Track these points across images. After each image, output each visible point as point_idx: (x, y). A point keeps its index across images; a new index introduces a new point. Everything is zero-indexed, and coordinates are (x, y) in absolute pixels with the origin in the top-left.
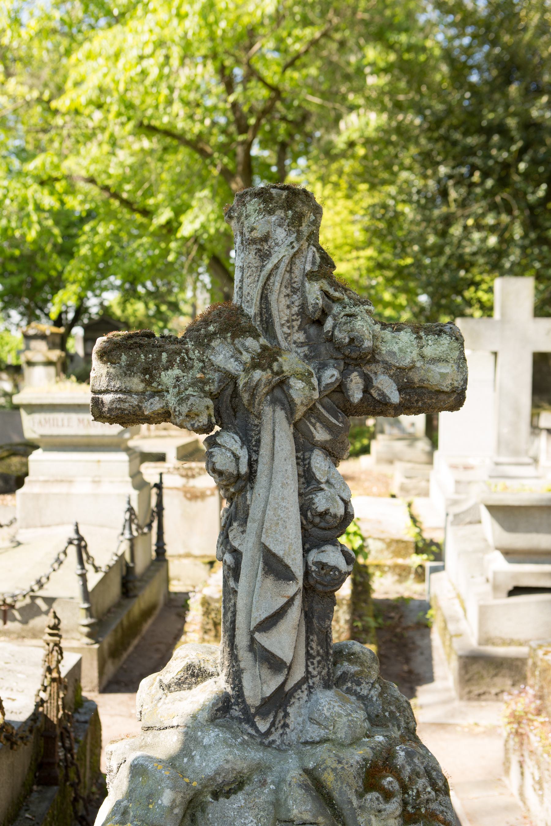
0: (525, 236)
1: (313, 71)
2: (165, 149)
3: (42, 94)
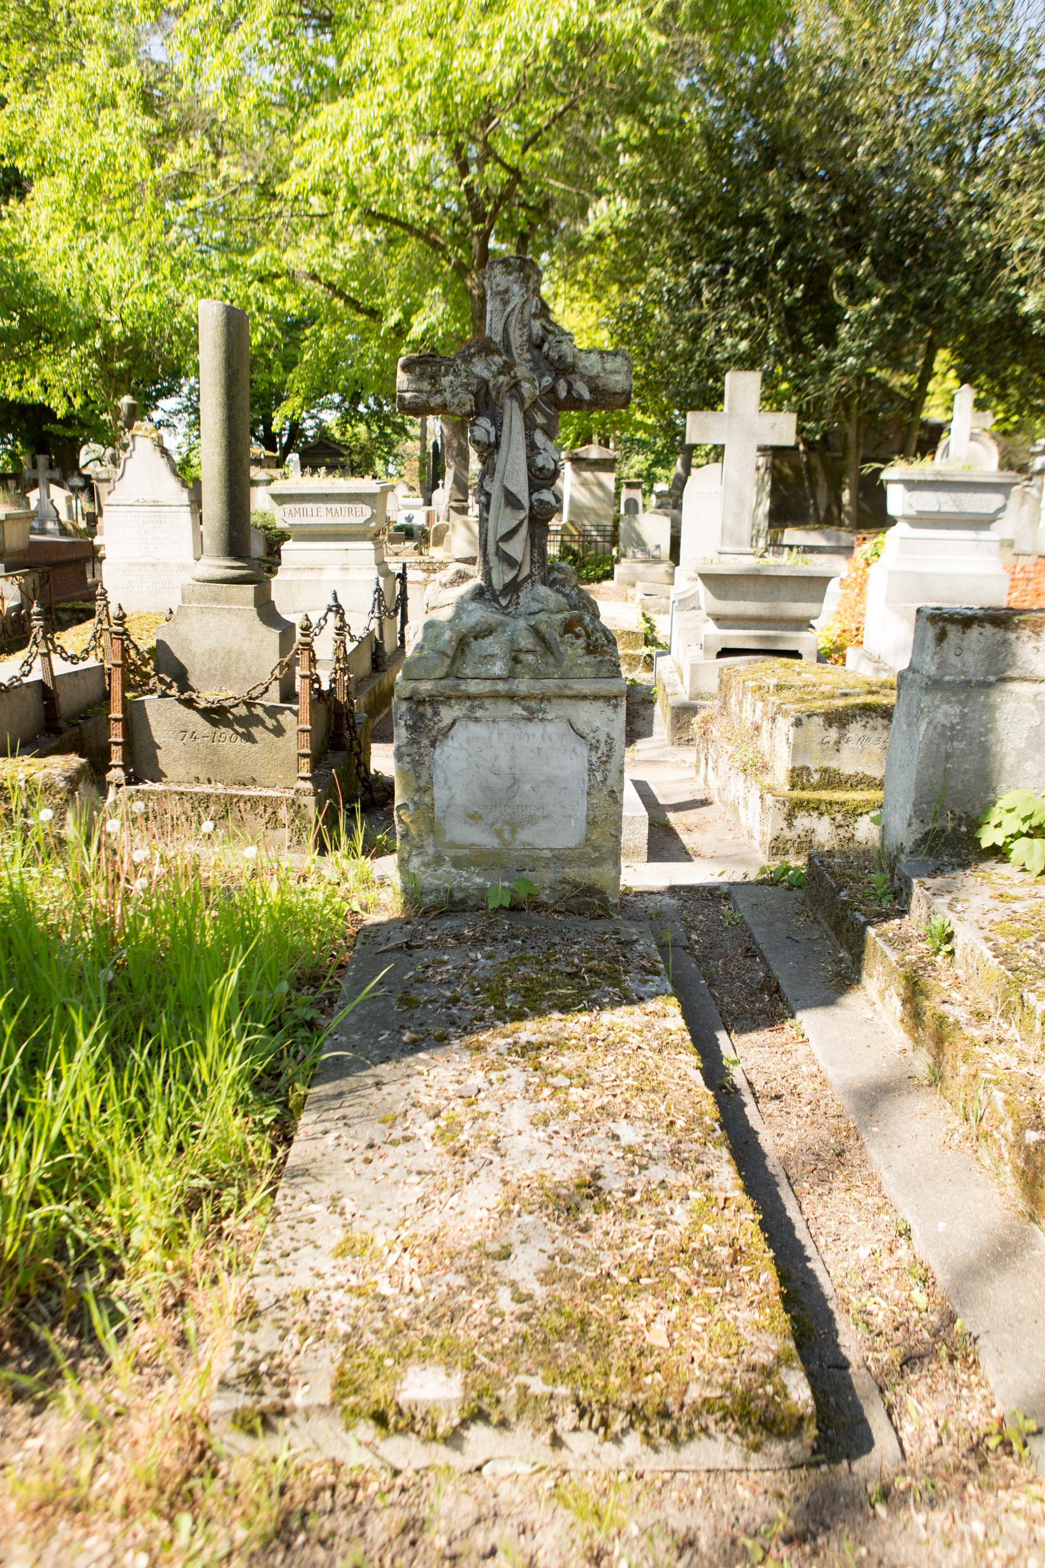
0: (782, 341)
1: (557, 151)
2: (391, 242)
3: (257, 177)
